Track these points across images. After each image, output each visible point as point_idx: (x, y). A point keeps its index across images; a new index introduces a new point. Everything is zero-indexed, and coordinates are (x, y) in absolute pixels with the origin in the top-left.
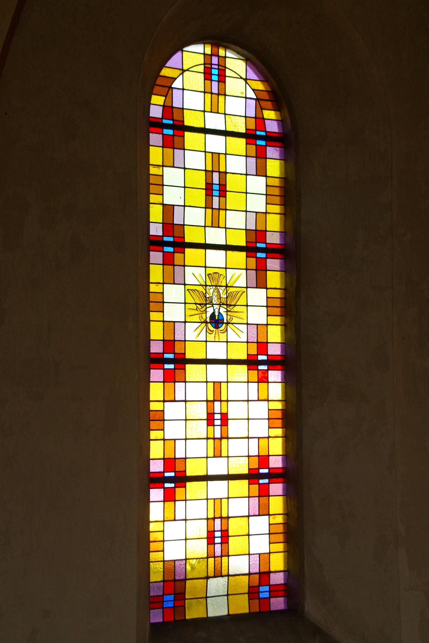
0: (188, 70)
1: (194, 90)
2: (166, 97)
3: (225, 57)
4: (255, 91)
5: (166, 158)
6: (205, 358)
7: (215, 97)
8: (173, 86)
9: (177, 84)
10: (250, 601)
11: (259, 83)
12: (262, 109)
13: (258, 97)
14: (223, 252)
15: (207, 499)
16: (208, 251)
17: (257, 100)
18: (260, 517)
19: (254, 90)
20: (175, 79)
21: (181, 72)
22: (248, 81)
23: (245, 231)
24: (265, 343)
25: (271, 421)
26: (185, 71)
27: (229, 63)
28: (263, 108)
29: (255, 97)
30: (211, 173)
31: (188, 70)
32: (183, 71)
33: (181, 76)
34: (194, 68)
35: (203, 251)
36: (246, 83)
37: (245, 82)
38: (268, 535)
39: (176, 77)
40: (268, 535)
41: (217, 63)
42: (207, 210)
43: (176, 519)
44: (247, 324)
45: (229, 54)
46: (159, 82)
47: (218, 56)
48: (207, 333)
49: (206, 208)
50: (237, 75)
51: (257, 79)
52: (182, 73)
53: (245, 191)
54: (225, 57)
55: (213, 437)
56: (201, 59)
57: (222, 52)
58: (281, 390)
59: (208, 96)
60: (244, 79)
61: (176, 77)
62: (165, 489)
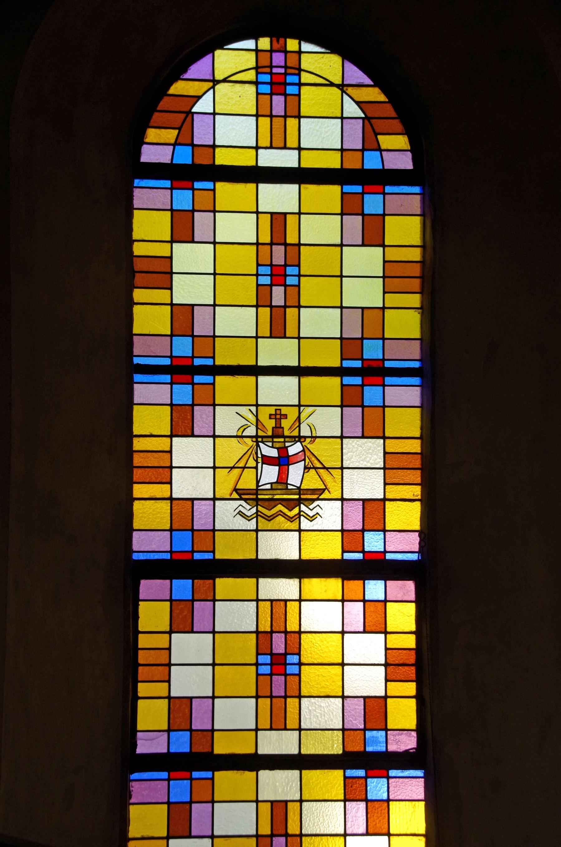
0: (225, 80)
2: (180, 129)
4: (360, 104)
7: (278, 122)
8: (194, 110)
9: (200, 107)
11: (377, 90)
12: (376, 134)
16: (261, 379)
17: (367, 119)
18: (255, 96)
19: (358, 103)
20: (199, 98)
21: (211, 84)
23: (339, 341)
25: (391, 668)
26: (219, 82)
27: (306, 62)
28: (378, 131)
29: (363, 116)
31: (225, 80)
32: (215, 82)
33: (212, 91)
34: (369, 126)
35: (250, 775)
36: (343, 92)
37: (340, 92)
39: (200, 94)
41: (283, 64)
44: (342, 500)
45: (306, 47)
46: (164, 104)
47: (286, 52)
48: (259, 430)
49: (257, 306)
50: (321, 79)
51: (372, 83)
52: (213, 87)
53: (339, 274)
54: (300, 52)
56: (250, 60)
57: (292, 44)
58: (415, 620)
59: (265, 122)
60: (337, 86)
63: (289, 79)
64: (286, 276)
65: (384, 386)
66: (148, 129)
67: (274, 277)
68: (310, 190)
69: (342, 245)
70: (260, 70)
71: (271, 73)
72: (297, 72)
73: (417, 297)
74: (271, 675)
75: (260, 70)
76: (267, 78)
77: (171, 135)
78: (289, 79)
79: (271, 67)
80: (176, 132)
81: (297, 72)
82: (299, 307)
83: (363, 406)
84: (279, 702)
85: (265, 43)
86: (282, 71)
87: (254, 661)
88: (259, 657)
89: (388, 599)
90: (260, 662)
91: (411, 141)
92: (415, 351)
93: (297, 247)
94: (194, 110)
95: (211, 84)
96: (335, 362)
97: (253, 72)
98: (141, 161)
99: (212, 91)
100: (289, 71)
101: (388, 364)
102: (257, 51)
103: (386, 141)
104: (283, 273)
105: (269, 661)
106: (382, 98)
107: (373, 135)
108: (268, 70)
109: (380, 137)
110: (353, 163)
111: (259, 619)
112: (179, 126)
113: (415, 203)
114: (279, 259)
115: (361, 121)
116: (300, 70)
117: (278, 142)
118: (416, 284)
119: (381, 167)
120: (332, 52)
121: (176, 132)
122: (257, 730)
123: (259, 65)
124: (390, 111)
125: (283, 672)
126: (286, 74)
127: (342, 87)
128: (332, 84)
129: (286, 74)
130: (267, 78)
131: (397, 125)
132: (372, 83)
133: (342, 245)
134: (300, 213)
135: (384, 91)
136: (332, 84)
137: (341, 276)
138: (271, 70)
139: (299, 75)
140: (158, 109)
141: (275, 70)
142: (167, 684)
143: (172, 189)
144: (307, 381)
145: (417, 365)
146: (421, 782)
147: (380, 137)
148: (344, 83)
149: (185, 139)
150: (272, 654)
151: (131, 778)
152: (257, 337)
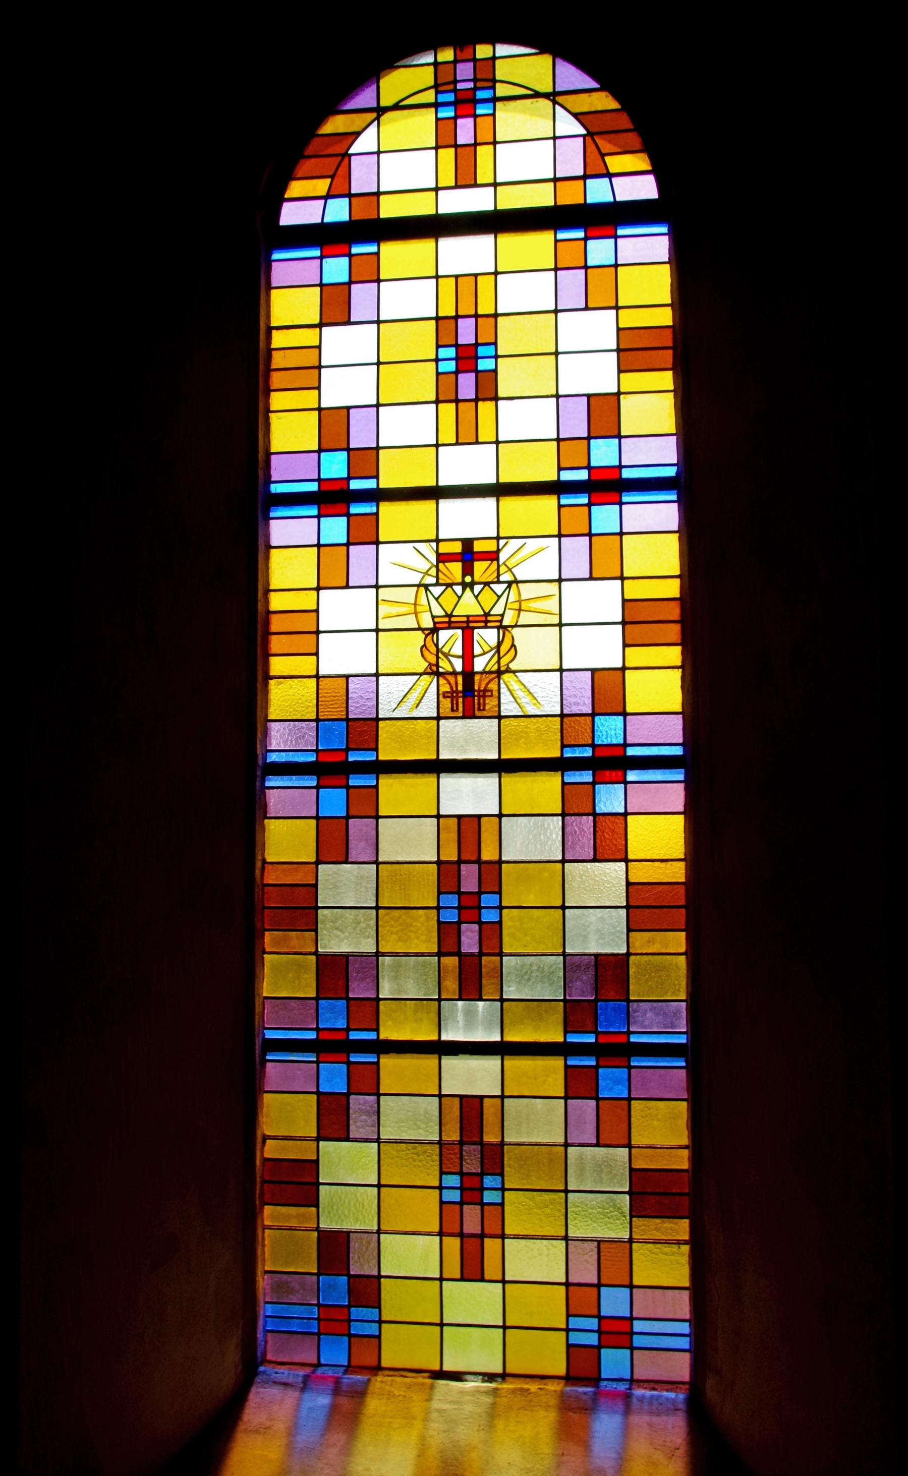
1: (413, 449)
2: (332, 177)
3: (494, 58)
5: (467, 1157)
6: (435, 484)
8: (350, 152)
10: (458, 1099)
12: (603, 156)
13: (592, 130)
14: (490, 503)
15: (437, 277)
16: (445, 243)
17: (590, 135)
19: (576, 116)
20: (357, 134)
22: (558, 99)
24: (454, 925)
27: (502, 70)
30: (453, 321)
36: (555, 103)
37: (551, 104)
38: (321, 629)
40: (321, 629)
42: (441, 151)
43: (499, 594)
45: (503, 50)
51: (597, 86)
52: (378, 119)
54: (494, 58)
55: (375, 105)
56: (426, 76)
57: (483, 51)
60: (546, 96)
61: (360, 130)
62: (592, 471)
63: (480, 95)
64: (482, 1189)
65: (621, 504)
66: (290, 183)
67: (463, 911)
68: (508, 241)
69: (556, 311)
70: (441, 89)
71: (455, 91)
72: (490, 84)
73: (669, 375)
74: (461, 1203)
75: (441, 89)
76: (450, 97)
77: (321, 186)
78: (480, 95)
79: (455, 82)
80: (329, 181)
81: (490, 84)
82: (503, 1236)
83: (589, 438)
84: (466, 308)
85: (447, 55)
86: (470, 85)
87: (436, 1183)
88: (440, 350)
89: (628, 742)
90: (440, 357)
91: (653, 160)
92: (674, 729)
93: (492, 320)
94: (350, 152)
95: (374, 115)
96: (549, 474)
97: (432, 92)
98: (281, 224)
99: (376, 122)
100: (479, 84)
101: (626, 474)
102: (436, 64)
103: (616, 163)
104: (476, 904)
105: (453, 355)
106: (613, 105)
107: (599, 157)
108: (451, 87)
109: (607, 159)
110: (571, 196)
111: (443, 1114)
112: (331, 173)
113: (676, 796)
114: (472, 1213)
115: (581, 139)
116: (494, 81)
117: (466, 285)
118: (674, 631)
119: (612, 200)
120: (542, 52)
121: (329, 181)
122: (441, 1279)
123: (439, 82)
124: (624, 122)
125: (479, 1201)
126: (475, 89)
127: (553, 96)
128: (537, 95)
129: (475, 89)
130: (450, 97)
131: (634, 140)
132: (597, 86)
133: (556, 311)
134: (496, 273)
135: (616, 96)
136: (537, 95)
137: (557, 354)
138: (456, 86)
139: (493, 88)
140: (306, 154)
141: (460, 86)
142: (314, 658)
143: (319, 517)
144: (508, 503)
145: (678, 751)
146: (665, 240)
147: (607, 159)
148: (556, 90)
149: (339, 189)
150: (456, 346)
151: (271, 516)
152: (437, 446)
